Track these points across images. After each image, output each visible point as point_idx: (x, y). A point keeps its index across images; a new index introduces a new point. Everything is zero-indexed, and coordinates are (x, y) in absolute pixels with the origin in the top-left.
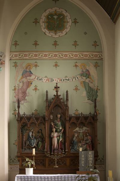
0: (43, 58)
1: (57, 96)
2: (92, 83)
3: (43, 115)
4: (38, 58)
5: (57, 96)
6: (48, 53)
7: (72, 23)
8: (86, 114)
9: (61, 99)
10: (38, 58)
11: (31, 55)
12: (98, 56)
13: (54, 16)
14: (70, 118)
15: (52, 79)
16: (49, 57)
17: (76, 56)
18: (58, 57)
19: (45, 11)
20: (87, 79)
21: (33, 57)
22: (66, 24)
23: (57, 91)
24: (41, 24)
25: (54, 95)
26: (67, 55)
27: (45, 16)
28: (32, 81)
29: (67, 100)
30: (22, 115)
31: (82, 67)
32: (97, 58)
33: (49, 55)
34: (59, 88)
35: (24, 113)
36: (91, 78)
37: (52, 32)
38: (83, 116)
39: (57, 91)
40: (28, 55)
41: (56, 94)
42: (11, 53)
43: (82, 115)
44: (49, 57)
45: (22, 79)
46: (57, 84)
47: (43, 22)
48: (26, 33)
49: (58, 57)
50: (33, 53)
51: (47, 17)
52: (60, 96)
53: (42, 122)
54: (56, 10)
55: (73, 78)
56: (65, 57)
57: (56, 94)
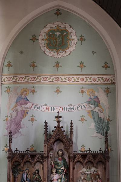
0: (42, 82)
1: (59, 128)
3: (41, 151)
4: (36, 82)
5: (59, 128)
6: (48, 76)
9: (64, 131)
10: (36, 82)
11: (27, 78)
15: (53, 108)
17: (82, 79)
20: (95, 107)
21: (30, 81)
23: (58, 122)
24: (40, 42)
25: (55, 127)
26: (59, 79)
30: (15, 151)
31: (90, 93)
33: (25, 79)
34: (61, 117)
35: (17, 148)
38: (91, 153)
39: (58, 122)
43: (89, 152)
44: (25, 80)
45: (15, 107)
46: (58, 112)
47: (43, 39)
50: (54, 76)
51: (48, 34)
52: (62, 127)
54: (58, 25)
55: (78, 107)
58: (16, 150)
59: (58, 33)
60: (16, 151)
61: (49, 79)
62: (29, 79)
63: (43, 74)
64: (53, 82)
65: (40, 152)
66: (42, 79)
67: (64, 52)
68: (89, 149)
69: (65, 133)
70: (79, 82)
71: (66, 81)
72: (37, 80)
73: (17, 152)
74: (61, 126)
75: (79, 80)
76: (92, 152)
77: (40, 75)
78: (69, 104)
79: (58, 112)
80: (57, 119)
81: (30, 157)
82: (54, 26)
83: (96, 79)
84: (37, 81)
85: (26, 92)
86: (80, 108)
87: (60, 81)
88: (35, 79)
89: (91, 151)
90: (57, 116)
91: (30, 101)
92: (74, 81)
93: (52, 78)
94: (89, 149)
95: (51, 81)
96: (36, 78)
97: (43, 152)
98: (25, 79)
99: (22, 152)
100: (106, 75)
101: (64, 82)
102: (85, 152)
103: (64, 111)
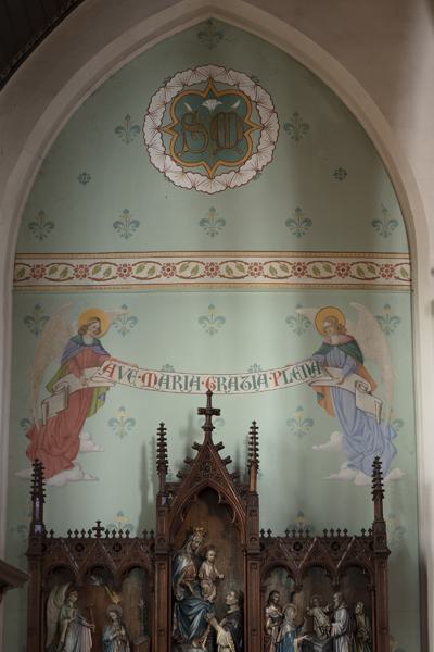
0: (156, 281)
2: (370, 393)
3: (325, 531)
5: (208, 452)
6: (92, 261)
7: (140, 125)
8: (335, 529)
9: (228, 460)
11: (148, 267)
12: (310, 267)
13: (205, 99)
14: (267, 542)
15: (153, 377)
16: (182, 277)
18: (354, 277)
19: (166, 83)
21: (158, 277)
22: (254, 135)
24: (148, 137)
27: (165, 104)
28: (108, 388)
29: (254, 464)
30: (90, 532)
32: (348, 280)
33: (181, 270)
34: (217, 412)
35: (99, 522)
36: (366, 376)
37: (193, 170)
39: (209, 428)
40: (178, 267)
41: (201, 441)
42: (18, 261)
43: (98, 535)
44: (183, 274)
45: (60, 378)
46: (210, 394)
47: (158, 129)
48: (340, 174)
49: (354, 277)
52: (220, 446)
53: (138, 562)
54: (211, 79)
55: (277, 374)
56: (340, 275)
57: (201, 441)
58: (94, 529)
59: (211, 104)
60: (95, 532)
61: (184, 268)
62: (152, 270)
63: (72, 255)
64: (152, 281)
65: (322, 535)
66: (71, 271)
67: (233, 173)
68: (96, 525)
69: (230, 468)
70: (333, 281)
71: (242, 277)
72: (94, 276)
73: (98, 535)
74: (215, 443)
75: (287, 271)
76: (107, 532)
77: (154, 255)
78: (165, 364)
79: (210, 394)
80: (204, 416)
81: (71, 551)
82: (193, 78)
83: (349, 269)
84: (182, 277)
85: (97, 324)
86: (281, 381)
87: (222, 276)
88: (174, 268)
89: (103, 529)
90: (204, 406)
91: (112, 356)
92: (226, 275)
93: (193, 265)
94: (96, 525)
95: (145, 279)
96: (178, 267)
97: (152, 532)
98: (181, 270)
99: (117, 535)
100: (291, 254)
101: (323, 278)
102: (301, 532)
103: (127, 382)
